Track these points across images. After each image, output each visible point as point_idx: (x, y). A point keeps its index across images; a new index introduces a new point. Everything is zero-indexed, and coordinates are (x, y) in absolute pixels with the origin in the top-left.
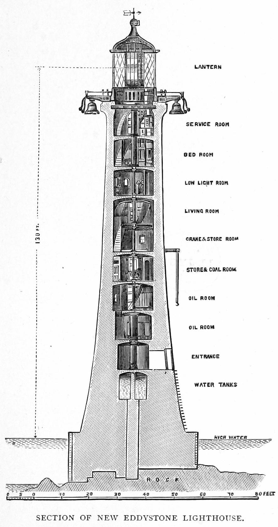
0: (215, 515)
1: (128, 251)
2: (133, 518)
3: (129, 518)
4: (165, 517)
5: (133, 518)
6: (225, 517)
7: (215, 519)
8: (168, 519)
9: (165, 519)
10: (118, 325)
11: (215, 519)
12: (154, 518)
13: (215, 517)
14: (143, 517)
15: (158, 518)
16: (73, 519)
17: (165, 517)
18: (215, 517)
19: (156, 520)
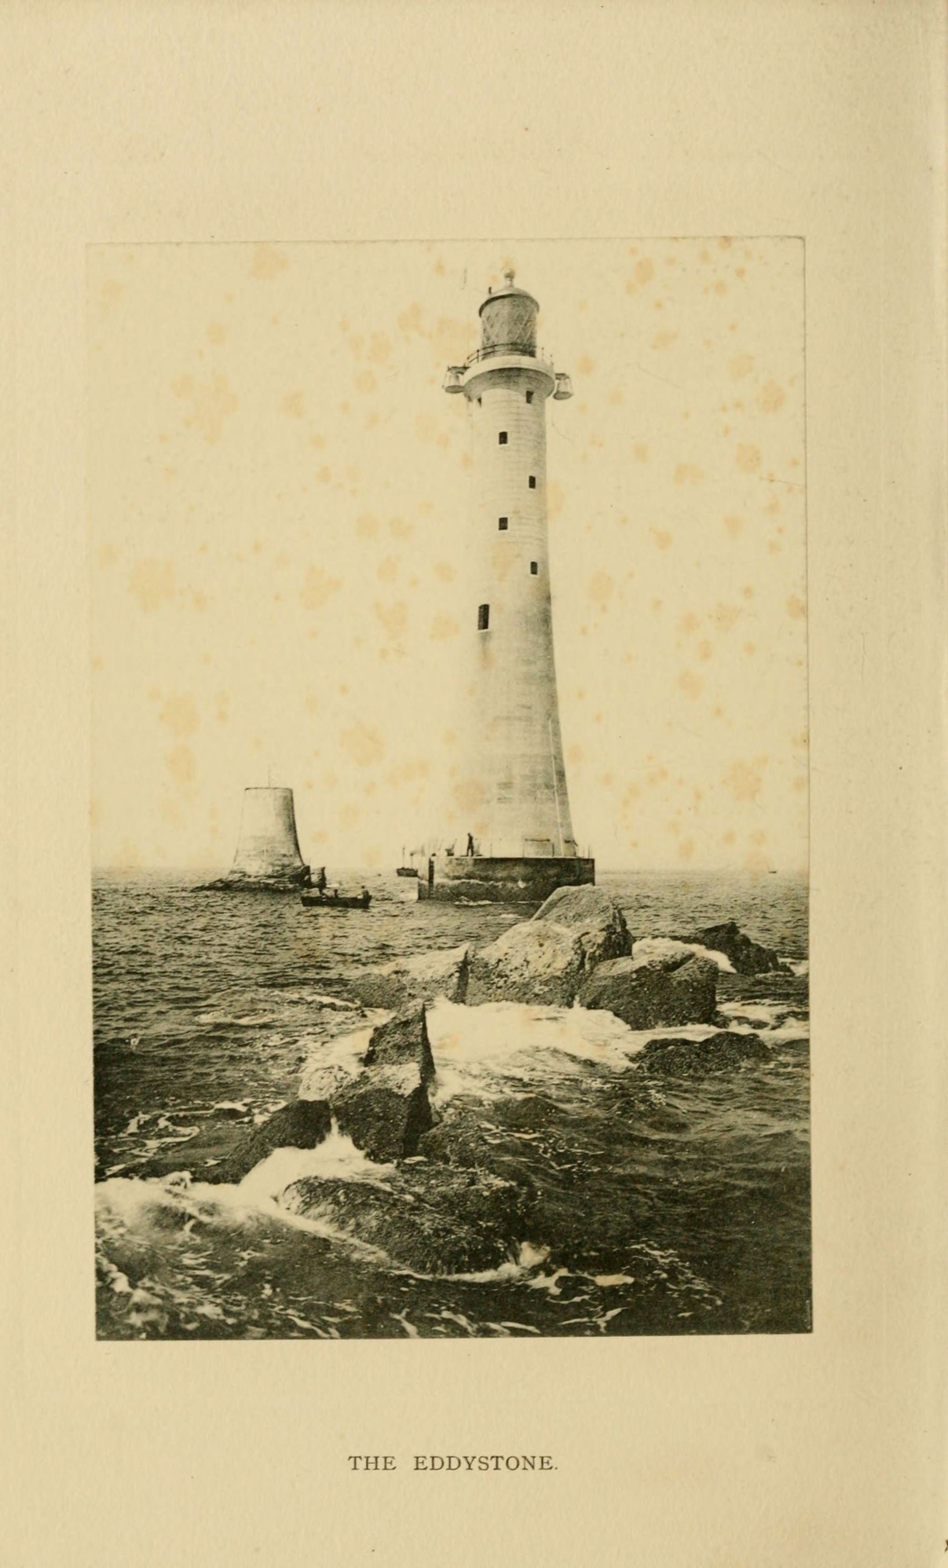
0: (372, 1454)
1: (658, 1219)
2: (438, 1463)
3: (428, 1463)
4: (522, 1461)
5: (438, 1463)
6: (446, 1461)
7: (372, 1466)
8: (528, 1466)
9: (522, 1466)
10: (509, 864)
11: (372, 1466)
12: (492, 1463)
13: (372, 1460)
14: (463, 1461)
15: (502, 1463)
16: (454, 390)
17: (522, 1461)
18: (372, 1460)
19: (497, 1468)
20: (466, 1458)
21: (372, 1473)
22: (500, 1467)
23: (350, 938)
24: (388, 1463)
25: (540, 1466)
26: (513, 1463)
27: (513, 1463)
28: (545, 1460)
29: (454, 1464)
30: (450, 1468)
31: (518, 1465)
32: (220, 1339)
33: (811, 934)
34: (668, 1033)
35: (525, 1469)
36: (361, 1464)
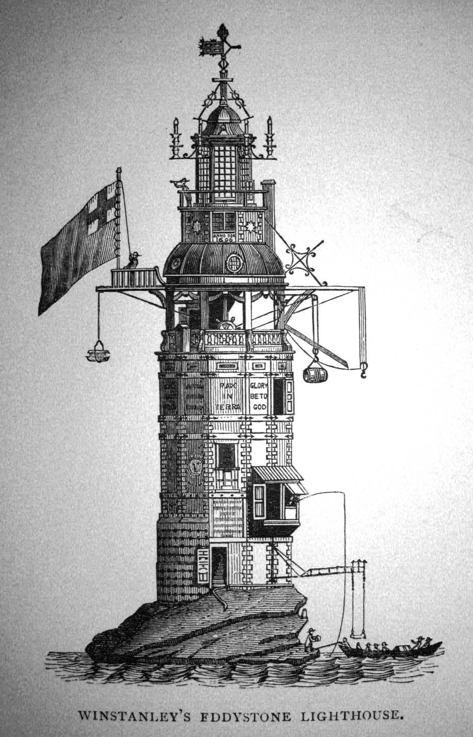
7: (356, 718)
8: (275, 719)
9: (270, 719)
11: (356, 718)
12: (252, 718)
15: (258, 717)
20: (235, 714)
21: (362, 721)
22: (347, 718)
23: (255, 117)
24: (286, 717)
25: (283, 719)
26: (264, 718)
27: (264, 718)
28: (164, 715)
29: (227, 717)
30: (224, 720)
31: (230, 719)
32: (137, 612)
33: (159, 482)
34: (271, 523)
35: (273, 721)
36: (349, 717)
